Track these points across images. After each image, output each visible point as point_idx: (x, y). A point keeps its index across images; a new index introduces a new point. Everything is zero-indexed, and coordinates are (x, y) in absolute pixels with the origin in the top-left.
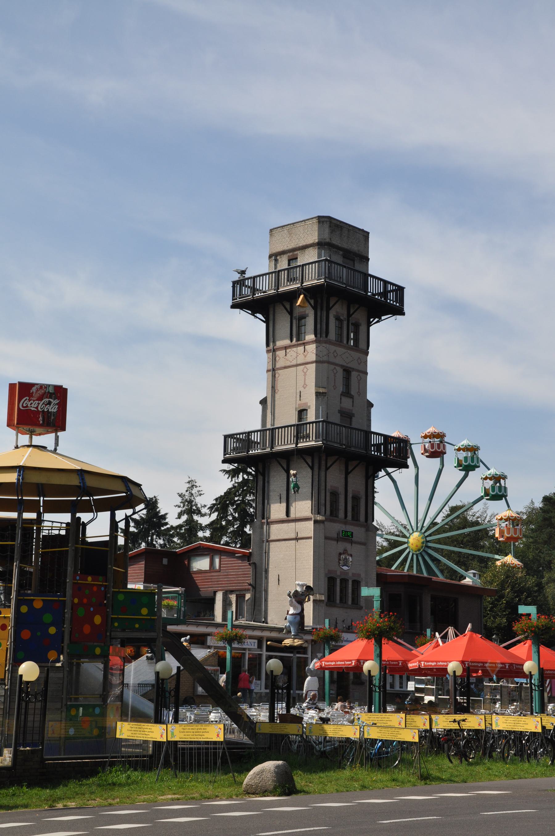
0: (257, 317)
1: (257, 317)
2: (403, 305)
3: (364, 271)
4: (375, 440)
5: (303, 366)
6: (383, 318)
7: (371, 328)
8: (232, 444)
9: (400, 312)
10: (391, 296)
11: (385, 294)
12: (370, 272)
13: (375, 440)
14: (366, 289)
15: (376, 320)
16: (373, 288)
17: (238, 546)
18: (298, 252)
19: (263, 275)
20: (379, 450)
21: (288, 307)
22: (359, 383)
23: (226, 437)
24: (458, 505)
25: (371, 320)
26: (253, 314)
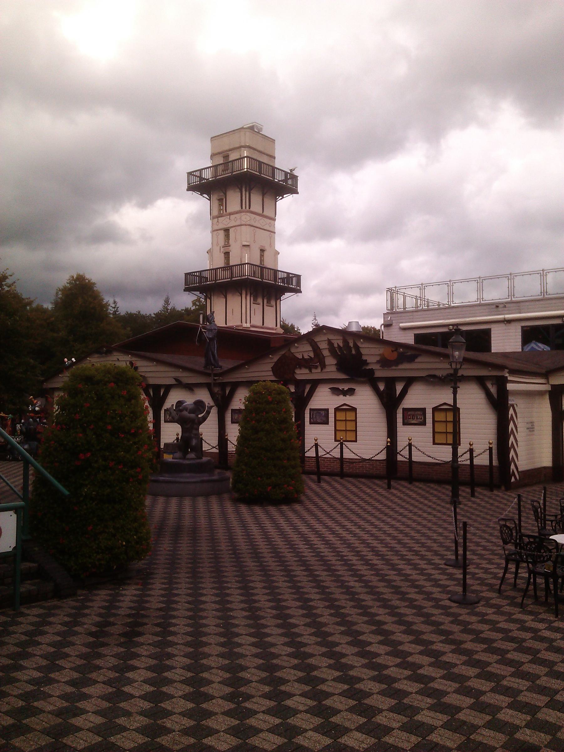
0: (204, 197)
1: (204, 197)
2: (297, 188)
3: (272, 164)
4: (280, 275)
5: (234, 228)
6: (285, 196)
7: (277, 203)
8: (439, 439)
9: (295, 192)
10: (290, 182)
11: (286, 180)
12: (277, 166)
13: (280, 275)
14: (273, 176)
15: (281, 197)
16: (279, 177)
17: (26, 447)
18: (230, 152)
19: (206, 168)
20: (283, 282)
21: (240, 292)
22: (270, 239)
23: (434, 443)
24: (142, 313)
25: (277, 197)
26: (201, 195)
